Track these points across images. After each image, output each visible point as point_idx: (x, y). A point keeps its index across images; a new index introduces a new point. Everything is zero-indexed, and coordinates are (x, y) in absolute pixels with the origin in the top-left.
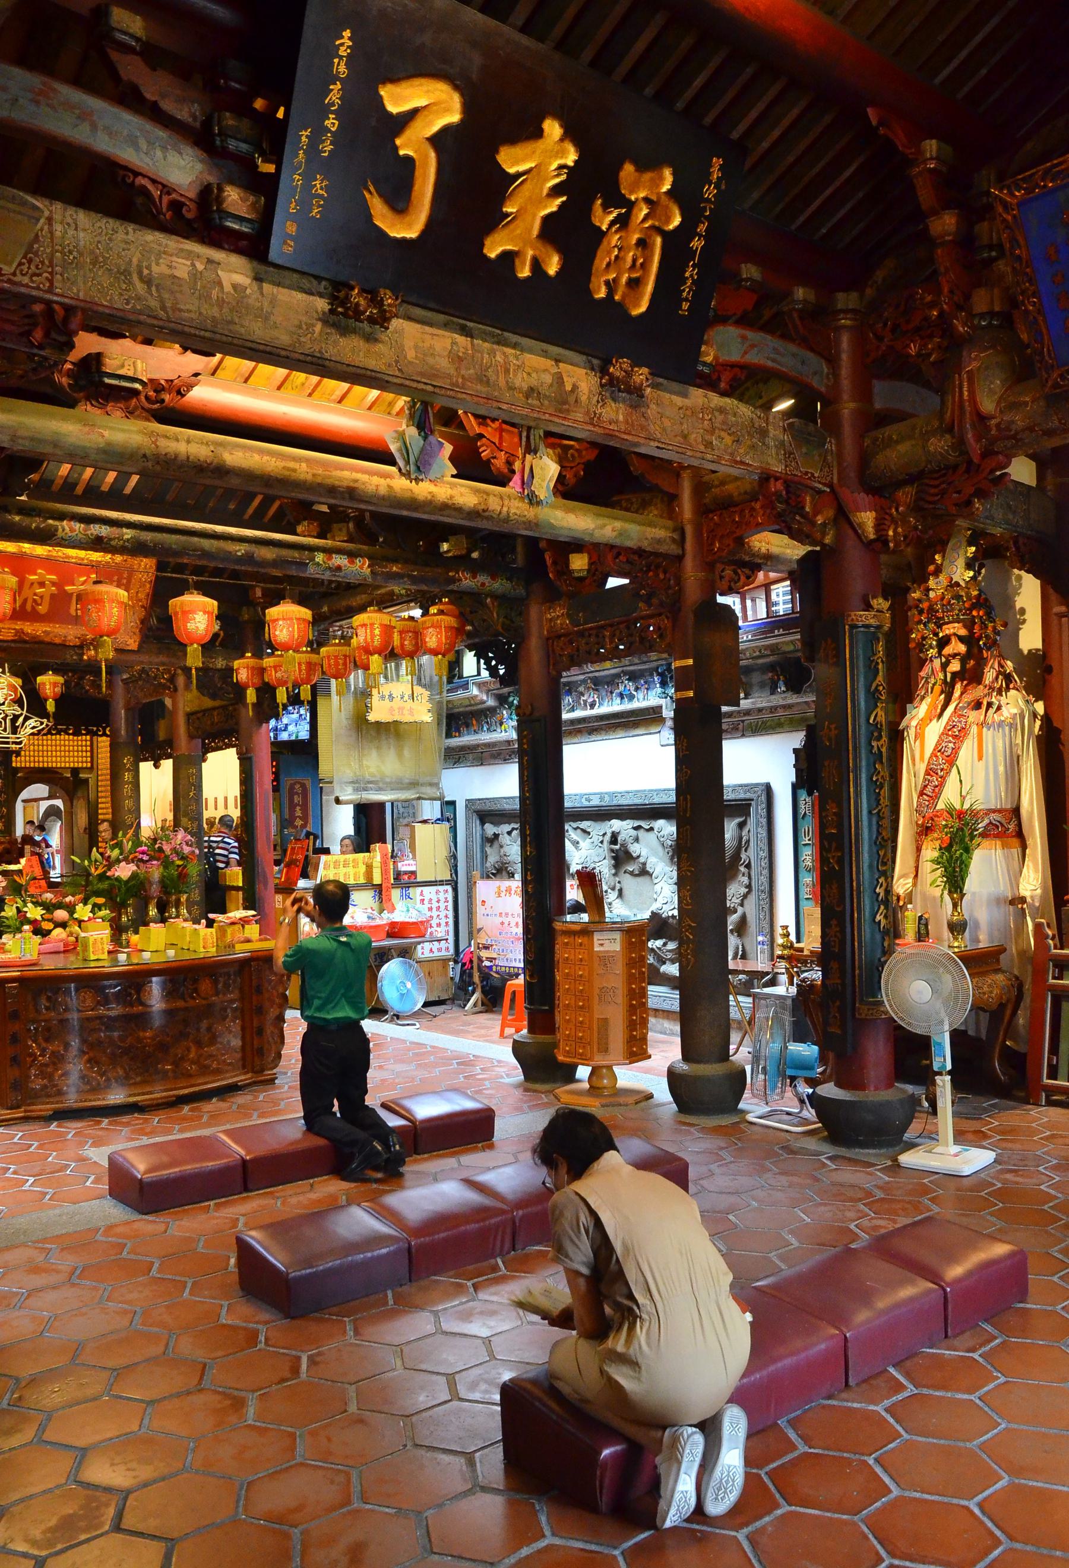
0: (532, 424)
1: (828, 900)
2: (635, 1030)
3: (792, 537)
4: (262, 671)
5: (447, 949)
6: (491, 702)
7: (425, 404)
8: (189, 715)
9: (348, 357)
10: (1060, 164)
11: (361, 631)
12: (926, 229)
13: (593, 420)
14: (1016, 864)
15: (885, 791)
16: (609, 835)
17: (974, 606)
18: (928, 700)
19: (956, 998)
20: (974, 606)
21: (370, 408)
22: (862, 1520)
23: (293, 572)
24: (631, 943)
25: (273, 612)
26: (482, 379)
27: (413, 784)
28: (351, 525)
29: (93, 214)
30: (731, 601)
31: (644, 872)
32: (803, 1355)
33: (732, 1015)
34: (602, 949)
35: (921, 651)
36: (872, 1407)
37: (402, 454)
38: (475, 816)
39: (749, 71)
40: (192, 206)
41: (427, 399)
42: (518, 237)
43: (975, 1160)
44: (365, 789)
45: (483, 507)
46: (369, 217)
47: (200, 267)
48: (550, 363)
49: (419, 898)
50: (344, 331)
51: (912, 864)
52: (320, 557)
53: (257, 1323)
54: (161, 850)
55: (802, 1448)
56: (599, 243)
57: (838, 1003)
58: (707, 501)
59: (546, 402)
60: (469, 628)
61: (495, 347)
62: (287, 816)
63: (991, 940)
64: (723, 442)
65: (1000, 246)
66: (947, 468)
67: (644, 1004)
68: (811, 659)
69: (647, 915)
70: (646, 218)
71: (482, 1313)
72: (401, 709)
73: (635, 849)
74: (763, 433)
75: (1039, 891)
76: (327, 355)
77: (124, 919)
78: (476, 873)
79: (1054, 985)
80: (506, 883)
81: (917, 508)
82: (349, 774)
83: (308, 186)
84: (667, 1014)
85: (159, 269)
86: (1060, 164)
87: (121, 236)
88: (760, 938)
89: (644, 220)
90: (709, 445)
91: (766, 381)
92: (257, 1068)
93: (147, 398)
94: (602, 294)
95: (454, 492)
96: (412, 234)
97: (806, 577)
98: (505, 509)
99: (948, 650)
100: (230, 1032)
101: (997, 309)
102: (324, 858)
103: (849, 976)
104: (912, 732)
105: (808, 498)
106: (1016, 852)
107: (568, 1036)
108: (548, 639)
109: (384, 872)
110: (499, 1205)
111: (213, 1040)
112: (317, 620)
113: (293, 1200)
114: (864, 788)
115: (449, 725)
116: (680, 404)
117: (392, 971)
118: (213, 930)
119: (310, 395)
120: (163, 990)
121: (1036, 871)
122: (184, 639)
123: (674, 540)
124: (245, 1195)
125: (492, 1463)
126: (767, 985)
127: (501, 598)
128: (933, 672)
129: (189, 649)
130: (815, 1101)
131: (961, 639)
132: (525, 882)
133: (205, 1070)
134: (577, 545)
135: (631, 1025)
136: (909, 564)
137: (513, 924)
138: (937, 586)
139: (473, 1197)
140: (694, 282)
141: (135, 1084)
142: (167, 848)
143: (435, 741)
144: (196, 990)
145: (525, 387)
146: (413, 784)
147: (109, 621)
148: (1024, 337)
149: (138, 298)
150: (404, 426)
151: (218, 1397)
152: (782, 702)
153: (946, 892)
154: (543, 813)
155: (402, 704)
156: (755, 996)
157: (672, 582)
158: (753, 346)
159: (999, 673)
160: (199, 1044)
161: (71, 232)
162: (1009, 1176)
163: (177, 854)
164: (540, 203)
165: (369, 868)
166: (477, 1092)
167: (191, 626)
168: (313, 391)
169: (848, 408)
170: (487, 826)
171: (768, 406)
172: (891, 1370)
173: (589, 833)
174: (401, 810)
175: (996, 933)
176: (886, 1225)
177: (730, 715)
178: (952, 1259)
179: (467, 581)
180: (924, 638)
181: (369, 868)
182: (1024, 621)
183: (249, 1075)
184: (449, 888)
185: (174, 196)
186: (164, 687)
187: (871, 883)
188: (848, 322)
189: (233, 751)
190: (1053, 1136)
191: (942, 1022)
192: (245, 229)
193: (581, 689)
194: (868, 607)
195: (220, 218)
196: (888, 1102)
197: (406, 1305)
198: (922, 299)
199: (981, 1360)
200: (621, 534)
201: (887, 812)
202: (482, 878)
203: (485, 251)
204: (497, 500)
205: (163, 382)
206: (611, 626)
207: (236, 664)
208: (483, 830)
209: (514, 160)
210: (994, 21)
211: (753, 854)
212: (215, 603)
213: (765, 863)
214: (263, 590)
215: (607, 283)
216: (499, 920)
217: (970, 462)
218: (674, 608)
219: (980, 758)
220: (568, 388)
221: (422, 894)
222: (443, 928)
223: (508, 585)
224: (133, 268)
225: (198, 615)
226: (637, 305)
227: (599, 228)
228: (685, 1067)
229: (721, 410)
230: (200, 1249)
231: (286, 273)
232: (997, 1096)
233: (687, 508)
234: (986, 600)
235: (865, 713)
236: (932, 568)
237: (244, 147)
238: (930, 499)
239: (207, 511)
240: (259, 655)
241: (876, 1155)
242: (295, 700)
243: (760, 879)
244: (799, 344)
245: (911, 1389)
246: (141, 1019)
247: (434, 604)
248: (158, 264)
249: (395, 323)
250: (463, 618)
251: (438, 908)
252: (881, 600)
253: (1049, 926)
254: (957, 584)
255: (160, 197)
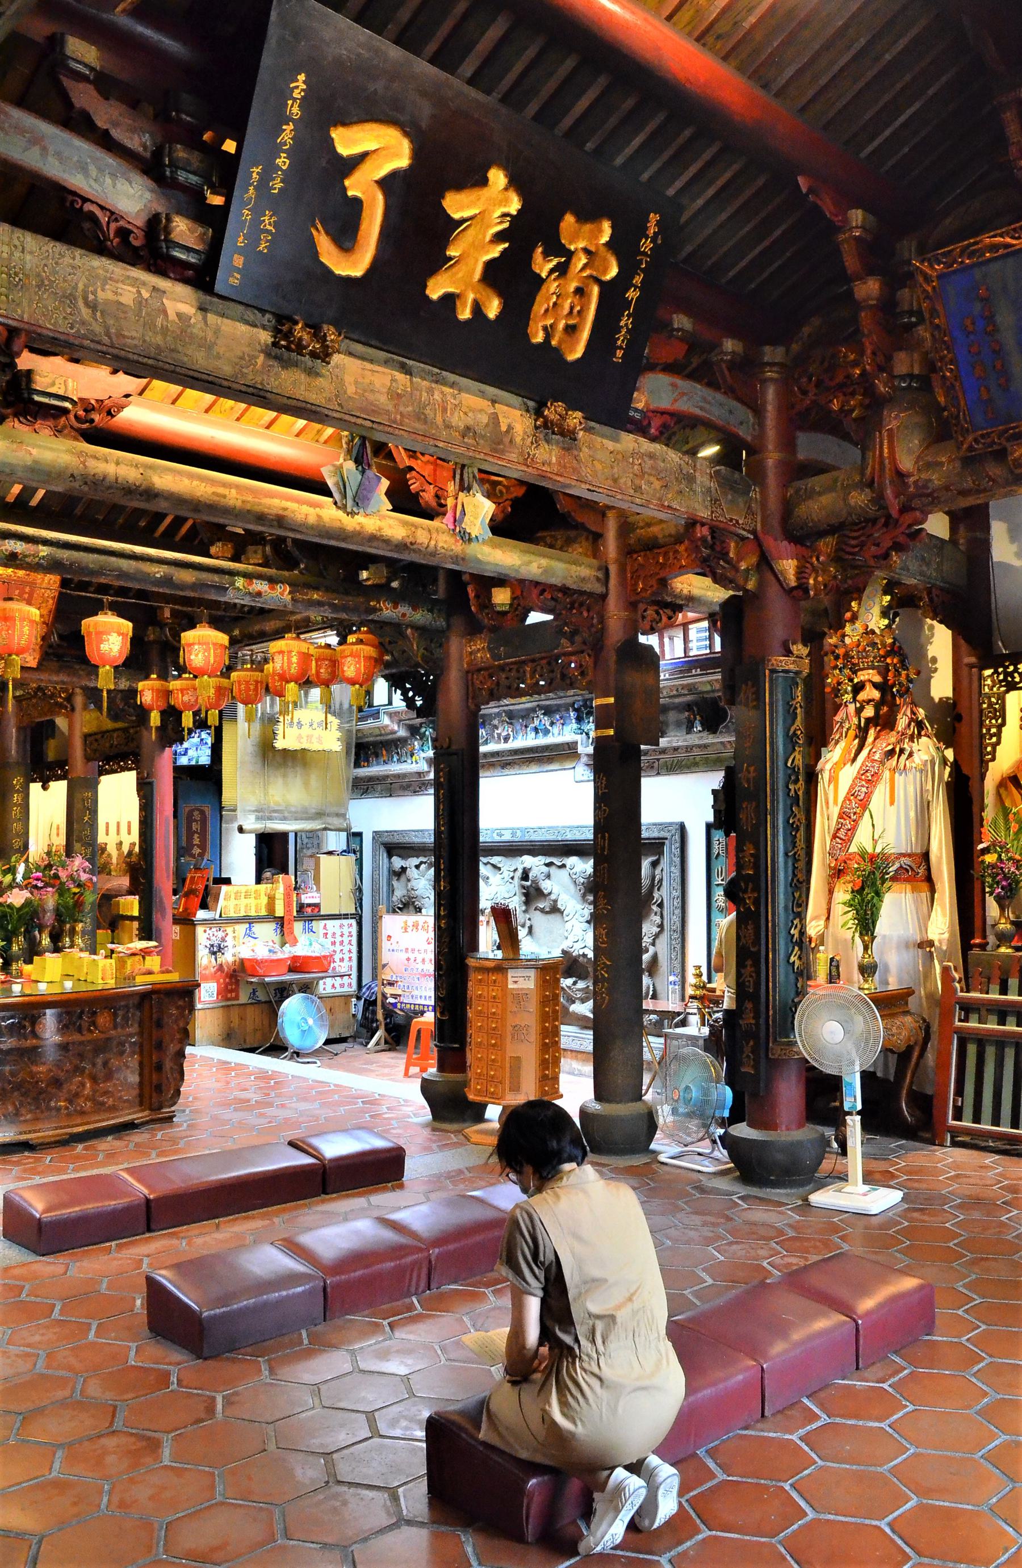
0: (466, 462)
1: (743, 941)
2: (548, 1069)
3: (716, 581)
4: (168, 693)
5: (350, 985)
6: (402, 733)
7: (363, 439)
8: (86, 737)
9: (288, 389)
10: (976, 243)
11: (278, 659)
12: (850, 294)
13: (527, 460)
14: (925, 908)
15: (801, 834)
16: (520, 871)
17: (888, 654)
18: (842, 744)
19: (867, 1040)
20: (888, 654)
21: (297, 435)
22: (780, 1542)
23: (213, 596)
24: (545, 981)
25: (188, 636)
26: (420, 416)
27: (319, 815)
28: (268, 548)
29: (40, 237)
30: (651, 640)
31: (555, 910)
32: (721, 1386)
33: (645, 1057)
34: (515, 986)
35: (837, 696)
36: (787, 1436)
37: (339, 488)
38: (382, 848)
39: (687, 133)
40: (140, 234)
41: (364, 434)
42: (460, 280)
43: (884, 1200)
44: (270, 818)
45: (411, 539)
46: (316, 254)
47: (146, 294)
48: (485, 404)
49: (322, 931)
50: (286, 364)
51: (825, 906)
52: (240, 582)
53: (170, 1364)
54: (56, 877)
55: (721, 1476)
56: (538, 288)
57: (751, 1043)
58: (632, 542)
59: (482, 442)
60: (387, 658)
61: (434, 385)
62: (184, 844)
63: (900, 981)
64: (651, 487)
65: (919, 313)
66: (867, 521)
67: (557, 1043)
68: (732, 702)
69: (557, 953)
70: (585, 267)
71: (398, 1351)
72: (309, 737)
73: (546, 886)
74: (691, 479)
75: (946, 936)
76: (268, 388)
77: (15, 948)
78: (382, 908)
79: (960, 1028)
80: (411, 919)
81: (837, 559)
82: (251, 803)
83: (256, 222)
84: (576, 1053)
85: (104, 295)
86: (976, 243)
87: (67, 260)
88: (672, 978)
89: (582, 270)
90: (638, 489)
91: (693, 427)
92: (156, 1105)
93: (76, 416)
94: (539, 338)
95: (383, 524)
96: (358, 272)
97: (729, 619)
98: (433, 543)
99: (862, 696)
100: (128, 1067)
101: (916, 371)
102: (224, 888)
103: (763, 1016)
104: (826, 775)
105: (732, 545)
106: (925, 895)
107: (480, 1074)
108: (467, 672)
109: (288, 905)
110: (415, 1243)
111: (109, 1076)
112: (233, 641)
113: (199, 1241)
114: (781, 830)
115: (357, 755)
116: (611, 448)
117: (293, 1008)
118: (113, 961)
119: (238, 419)
120: (59, 1022)
121: (944, 915)
122: (94, 659)
123: (598, 579)
124: (147, 1235)
125: (416, 1498)
126: (677, 1026)
127: (422, 630)
128: (847, 716)
129: (101, 670)
130: (727, 1141)
131: (875, 686)
132: (438, 917)
133: (100, 1107)
134: (500, 581)
135: (544, 1064)
136: (826, 610)
137: (419, 960)
138: (852, 633)
139: (389, 1236)
140: (628, 331)
141: (25, 1121)
142: (63, 875)
143: (344, 771)
144: (94, 1023)
145: (462, 425)
146: (319, 815)
147: (19, 640)
148: (942, 400)
149: (83, 323)
150: (341, 460)
151: (133, 1439)
152: (697, 742)
153: (857, 935)
154: (458, 847)
155: (310, 731)
156: (666, 1036)
157: (595, 621)
158: (683, 394)
159: (911, 720)
160: (94, 1079)
161: (17, 254)
162: (916, 1215)
163: (74, 881)
164: (482, 248)
165: (271, 900)
166: (384, 1131)
167: (104, 647)
168: (242, 415)
169: (772, 459)
170: (395, 859)
171: (693, 452)
172: (805, 1401)
173: (499, 869)
174: (305, 841)
175: (906, 977)
176: (796, 1261)
177: (646, 753)
178: (864, 1290)
179: (388, 611)
180: (839, 684)
181: (271, 900)
182: (936, 670)
183: (146, 1113)
184: (353, 922)
185: (122, 223)
186: (61, 706)
187: (786, 924)
188: (775, 375)
189: (133, 774)
190: (957, 1176)
191: (852, 1063)
192: (192, 259)
193: (496, 722)
194: (788, 653)
195: (168, 248)
196: (800, 1143)
197: (321, 1345)
198: (845, 356)
199: (890, 1390)
200: (546, 571)
201: (802, 853)
202: (388, 912)
203: (427, 292)
204: (425, 533)
205: (93, 402)
206: (533, 661)
207: (141, 685)
208: (390, 863)
209: (458, 205)
210: (917, 105)
211: (666, 893)
212: (130, 624)
213: (677, 903)
214: (172, 611)
215: (545, 329)
216: (404, 956)
217: (889, 517)
218: (596, 646)
219: (892, 803)
220: (504, 428)
221: (325, 927)
222: (346, 963)
223: (429, 616)
224: (79, 293)
225: (110, 636)
226: (572, 350)
227: (539, 276)
228: (596, 1107)
229: (651, 456)
230: (103, 1291)
231: (232, 304)
232: (907, 1138)
233: (611, 546)
234: (900, 648)
235: (783, 756)
236: (848, 615)
237: (194, 179)
238: (849, 549)
239: (117, 527)
240: (164, 676)
241: (787, 1195)
242: (201, 724)
243: (672, 919)
244: (725, 393)
245: (824, 1419)
246: (32, 1054)
247: (351, 632)
248: (103, 290)
249: (337, 358)
250: (382, 647)
251: (342, 942)
252: (800, 646)
253: (956, 969)
254: (873, 632)
255: (108, 223)
